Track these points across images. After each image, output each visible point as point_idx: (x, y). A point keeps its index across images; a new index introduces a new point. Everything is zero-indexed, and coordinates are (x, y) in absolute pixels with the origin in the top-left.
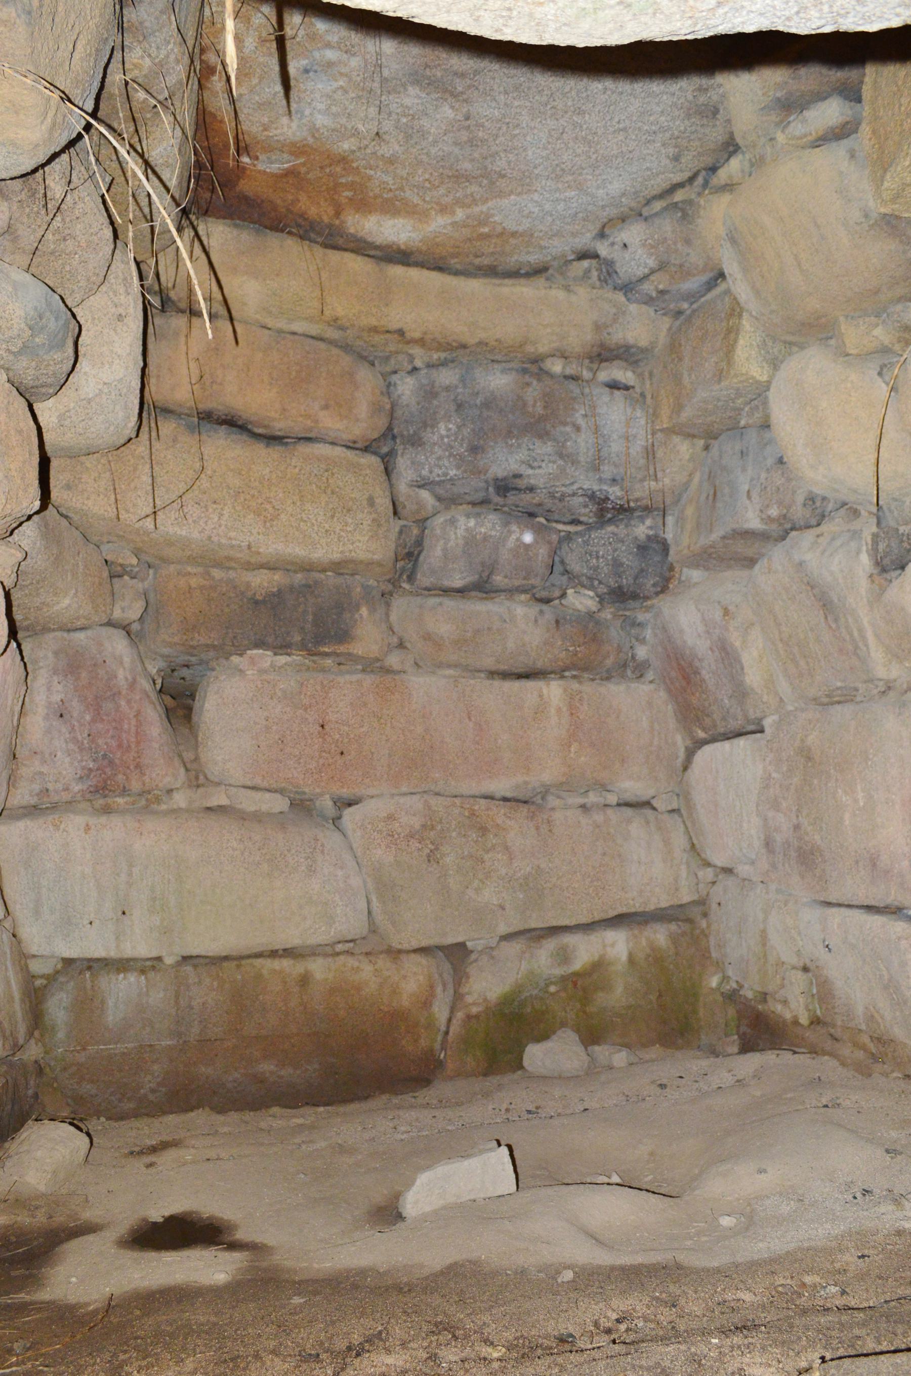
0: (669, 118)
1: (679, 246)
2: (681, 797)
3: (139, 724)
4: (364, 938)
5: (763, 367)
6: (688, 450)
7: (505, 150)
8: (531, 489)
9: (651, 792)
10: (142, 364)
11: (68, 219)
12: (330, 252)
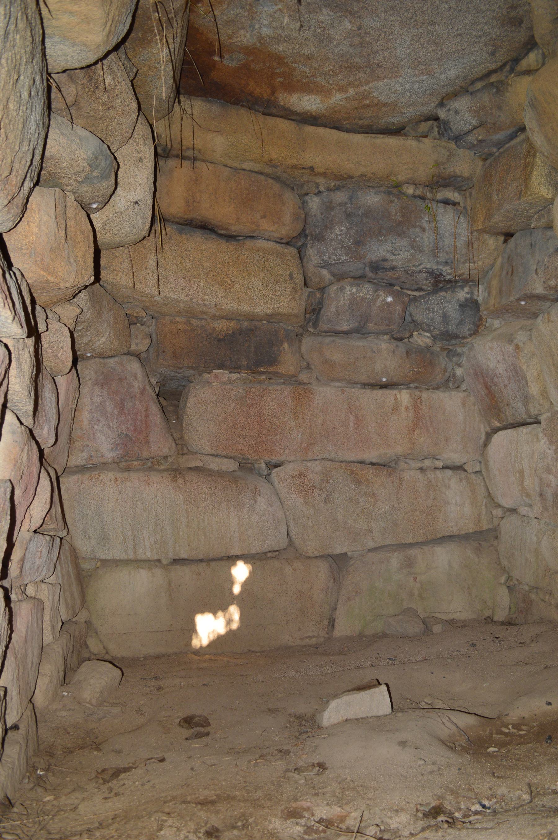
0: (490, 27)
1: (494, 111)
2: (482, 464)
3: (147, 416)
4: (284, 549)
5: (549, 189)
6: (493, 243)
7: (383, 50)
8: (393, 268)
9: (464, 460)
10: (153, 189)
11: (111, 96)
12: (267, 117)
